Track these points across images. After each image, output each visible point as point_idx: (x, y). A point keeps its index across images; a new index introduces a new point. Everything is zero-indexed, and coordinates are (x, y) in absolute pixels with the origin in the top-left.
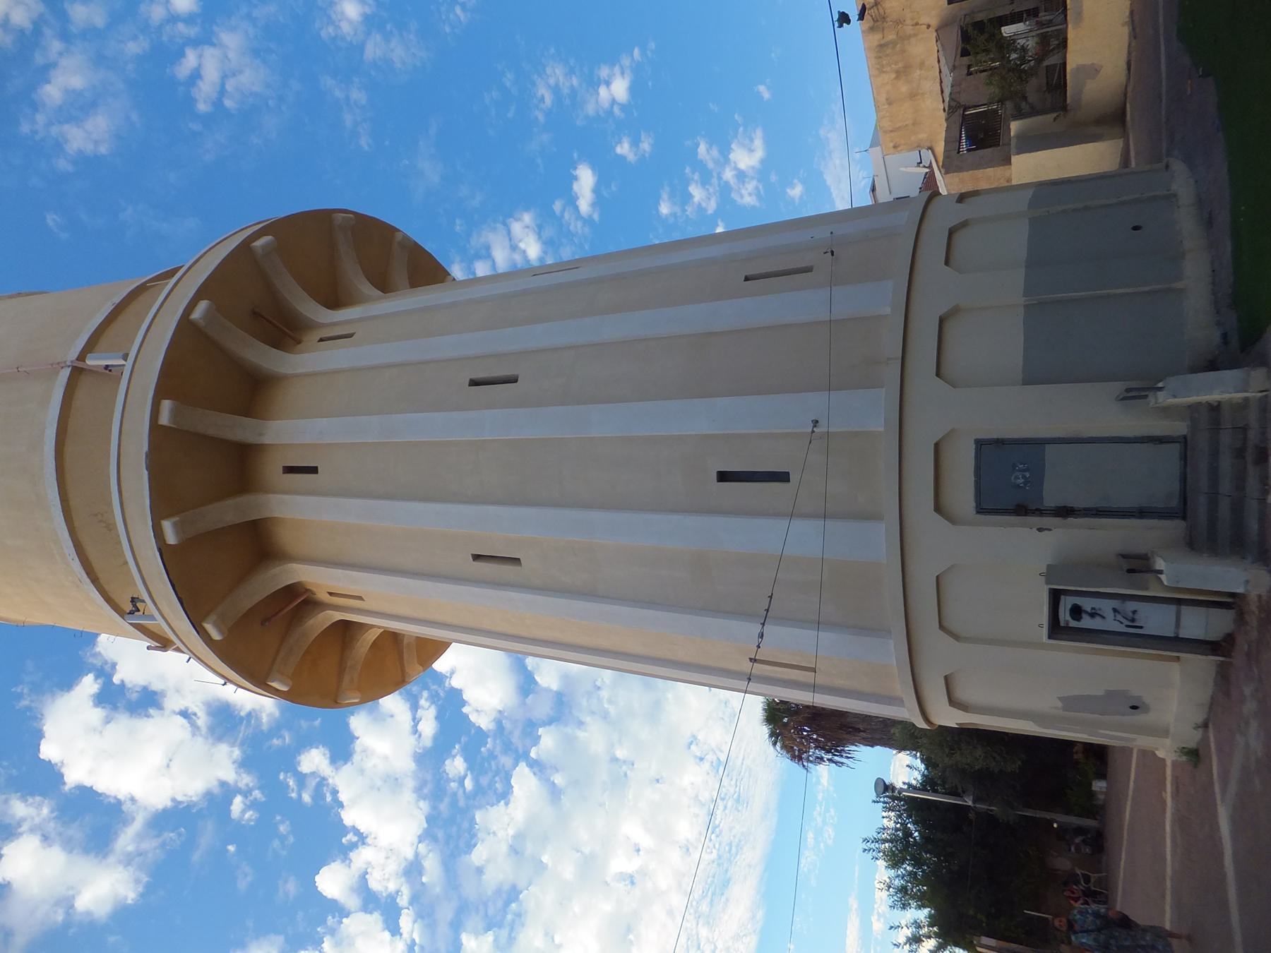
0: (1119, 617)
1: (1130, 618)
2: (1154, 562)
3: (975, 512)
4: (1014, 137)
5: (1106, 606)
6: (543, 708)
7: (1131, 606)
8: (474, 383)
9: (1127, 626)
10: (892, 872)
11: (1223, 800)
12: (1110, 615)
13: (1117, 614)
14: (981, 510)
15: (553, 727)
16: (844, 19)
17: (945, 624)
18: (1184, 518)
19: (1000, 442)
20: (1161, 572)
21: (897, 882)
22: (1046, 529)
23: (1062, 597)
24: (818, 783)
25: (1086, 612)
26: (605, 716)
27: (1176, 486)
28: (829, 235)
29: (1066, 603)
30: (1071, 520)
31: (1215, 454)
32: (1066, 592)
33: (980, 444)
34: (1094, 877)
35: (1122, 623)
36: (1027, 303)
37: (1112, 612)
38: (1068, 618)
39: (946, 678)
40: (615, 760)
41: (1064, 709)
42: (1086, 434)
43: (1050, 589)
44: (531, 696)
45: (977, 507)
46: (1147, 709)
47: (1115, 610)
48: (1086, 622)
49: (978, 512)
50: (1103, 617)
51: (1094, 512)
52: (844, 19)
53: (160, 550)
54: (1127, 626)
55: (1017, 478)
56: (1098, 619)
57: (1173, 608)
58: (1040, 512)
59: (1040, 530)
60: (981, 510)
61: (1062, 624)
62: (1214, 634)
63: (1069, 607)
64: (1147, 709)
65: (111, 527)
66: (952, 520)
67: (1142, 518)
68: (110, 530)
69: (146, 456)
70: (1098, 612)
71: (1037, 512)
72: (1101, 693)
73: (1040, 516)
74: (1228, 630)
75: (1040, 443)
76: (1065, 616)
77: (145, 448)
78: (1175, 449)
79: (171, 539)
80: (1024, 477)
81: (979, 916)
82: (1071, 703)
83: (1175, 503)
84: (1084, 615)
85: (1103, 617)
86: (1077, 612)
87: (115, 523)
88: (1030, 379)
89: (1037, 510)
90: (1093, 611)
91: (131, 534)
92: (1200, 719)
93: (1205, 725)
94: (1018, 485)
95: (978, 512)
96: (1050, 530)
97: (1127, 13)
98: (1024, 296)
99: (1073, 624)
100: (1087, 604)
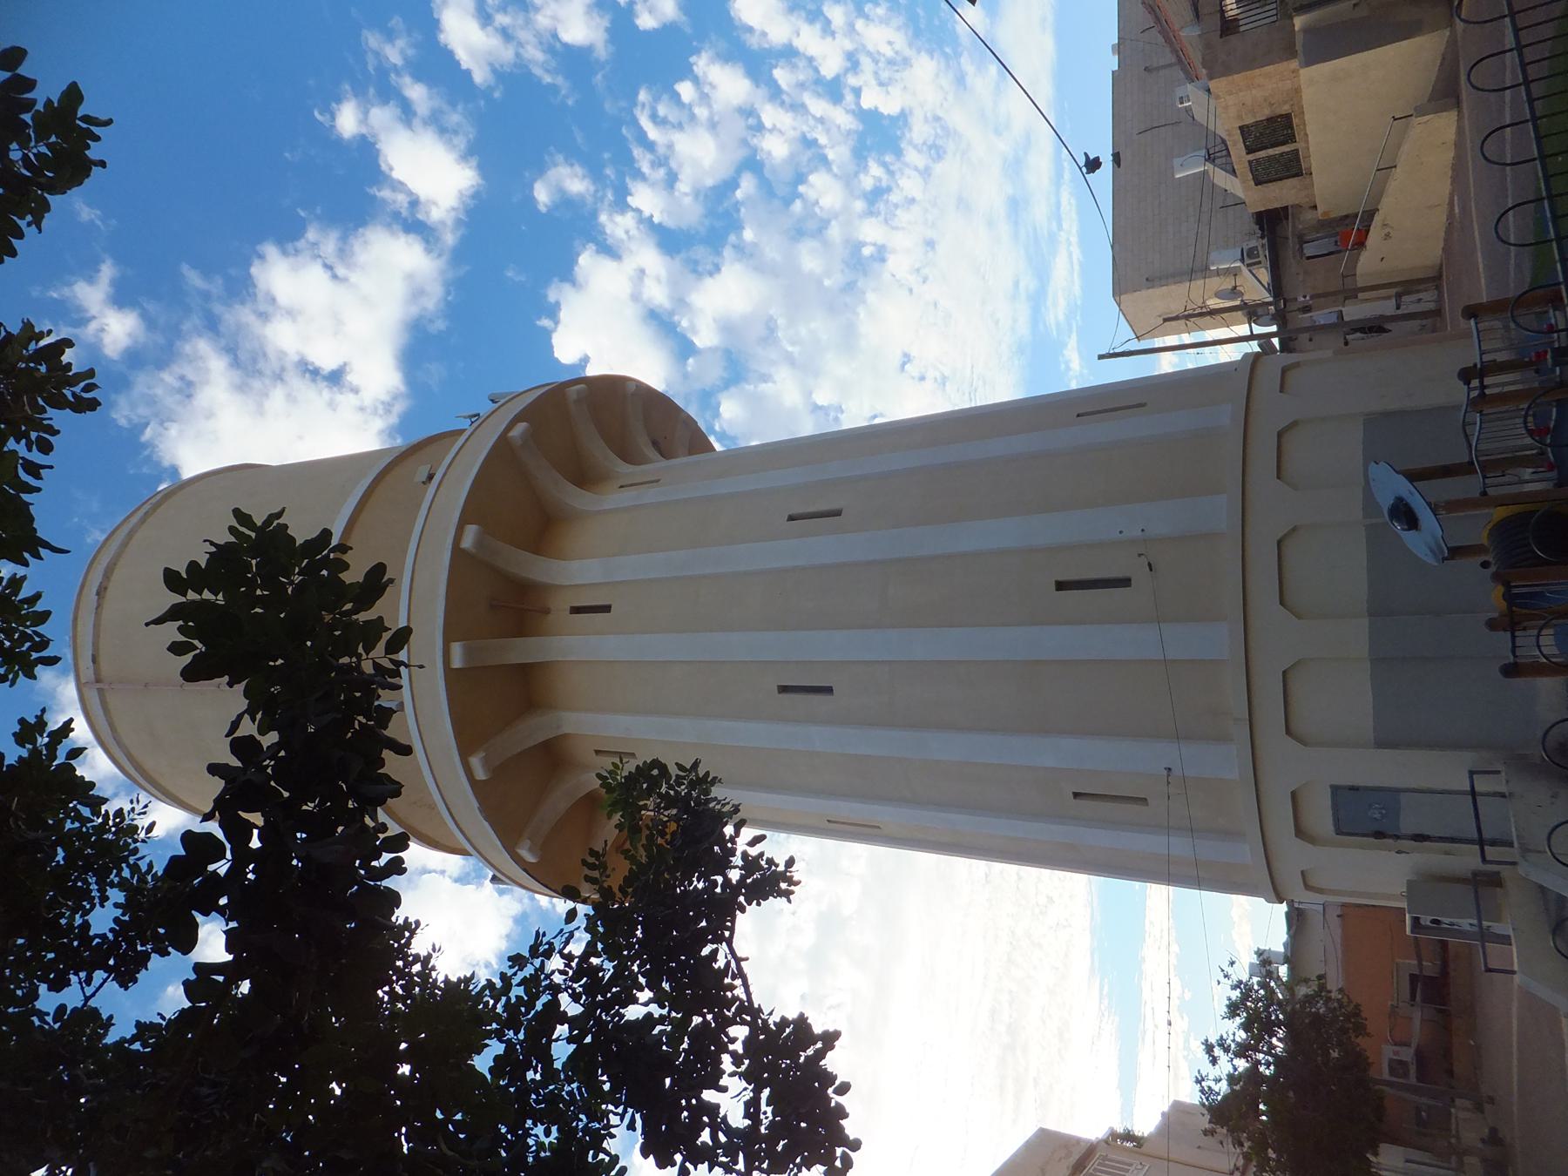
4: (1299, 31)
6: (714, 373)
8: (784, 689)
14: (1339, 832)
15: (733, 390)
16: (1093, 165)
17: (1310, 883)
19: (1354, 789)
24: (1068, 369)
26: (791, 360)
28: (1140, 533)
30: (1427, 844)
33: (1335, 790)
39: (1294, 795)
40: (816, 408)
44: (691, 361)
45: (1336, 830)
52: (1093, 165)
53: (525, 870)
58: (1397, 837)
60: (1339, 832)
65: (432, 807)
68: (433, 808)
69: (480, 812)
75: (1398, 791)
77: (475, 804)
79: (530, 858)
87: (434, 802)
88: (1381, 744)
91: (492, 861)
94: (1375, 818)
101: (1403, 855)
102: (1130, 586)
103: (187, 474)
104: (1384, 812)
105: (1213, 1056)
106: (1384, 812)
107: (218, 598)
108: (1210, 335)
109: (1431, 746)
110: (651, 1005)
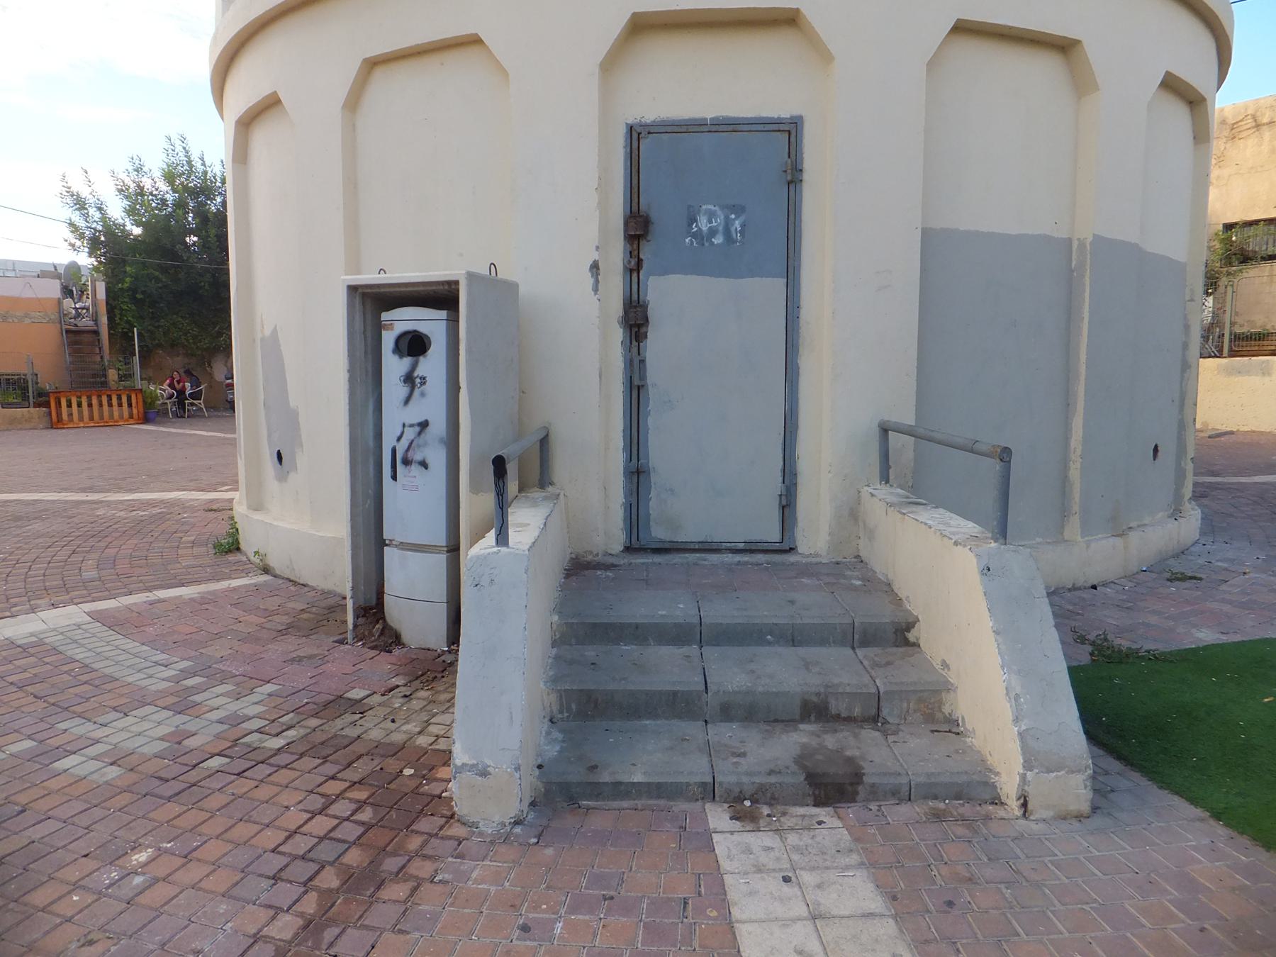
0: (410, 434)
1: (410, 454)
2: (534, 504)
3: (630, 122)
5: (432, 405)
7: (437, 457)
9: (394, 451)
10: (157, 174)
11: (97, 617)
12: (414, 414)
13: (417, 429)
14: (636, 134)
17: (379, 73)
18: (628, 549)
19: (793, 177)
20: (502, 539)
21: (147, 184)
22: (597, 281)
23: (443, 314)
25: (414, 367)
27: (690, 534)
29: (430, 322)
30: (618, 334)
31: (793, 637)
32: (453, 321)
33: (791, 130)
34: (201, 403)
35: (399, 439)
36: (1075, 245)
37: (421, 419)
38: (400, 328)
41: (262, 339)
42: (806, 363)
43: (457, 283)
46: (282, 478)
47: (424, 425)
48: (394, 366)
49: (631, 128)
50: (407, 401)
51: (636, 382)
54: (394, 451)
55: (711, 216)
56: (403, 390)
57: (441, 539)
58: (634, 268)
59: (595, 267)
60: (636, 134)
61: (385, 316)
62: (395, 611)
63: (423, 328)
64: (282, 478)
66: (612, 62)
67: (625, 477)
70: (417, 392)
71: (633, 262)
72: (292, 404)
73: (625, 267)
74: (406, 637)
76: (404, 319)
78: (771, 533)
80: (713, 232)
81: (128, 279)
82: (273, 346)
83: (659, 533)
84: (407, 361)
85: (407, 401)
86: (414, 345)
89: (639, 262)
90: (418, 380)
92: (273, 562)
93: (266, 570)
95: (631, 128)
96: (596, 290)
97: (1224, 428)
98: (1098, 239)
99: (388, 339)
100: (432, 365)
101: (590, 281)
102: (1168, 74)
103: (383, 332)
104: (718, 240)
105: (444, 703)
106: (718, 240)
107: (155, 205)
108: (729, 545)
109: (924, 270)
110: (706, 807)
